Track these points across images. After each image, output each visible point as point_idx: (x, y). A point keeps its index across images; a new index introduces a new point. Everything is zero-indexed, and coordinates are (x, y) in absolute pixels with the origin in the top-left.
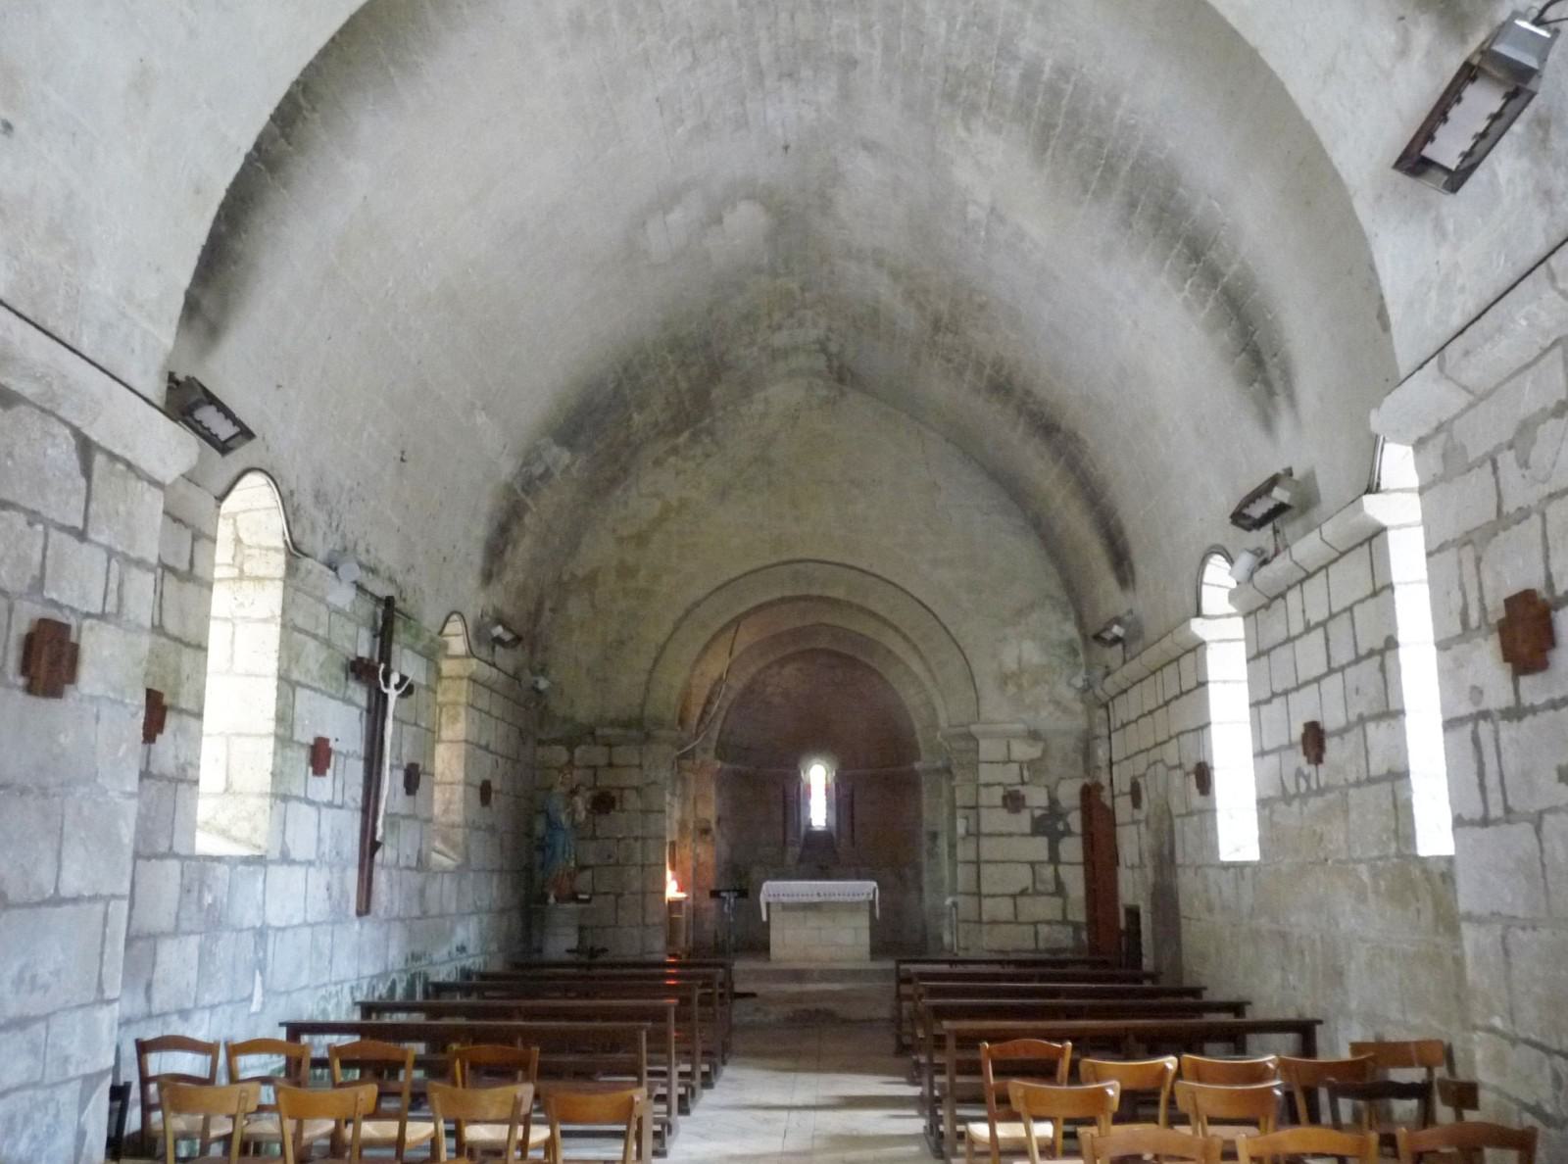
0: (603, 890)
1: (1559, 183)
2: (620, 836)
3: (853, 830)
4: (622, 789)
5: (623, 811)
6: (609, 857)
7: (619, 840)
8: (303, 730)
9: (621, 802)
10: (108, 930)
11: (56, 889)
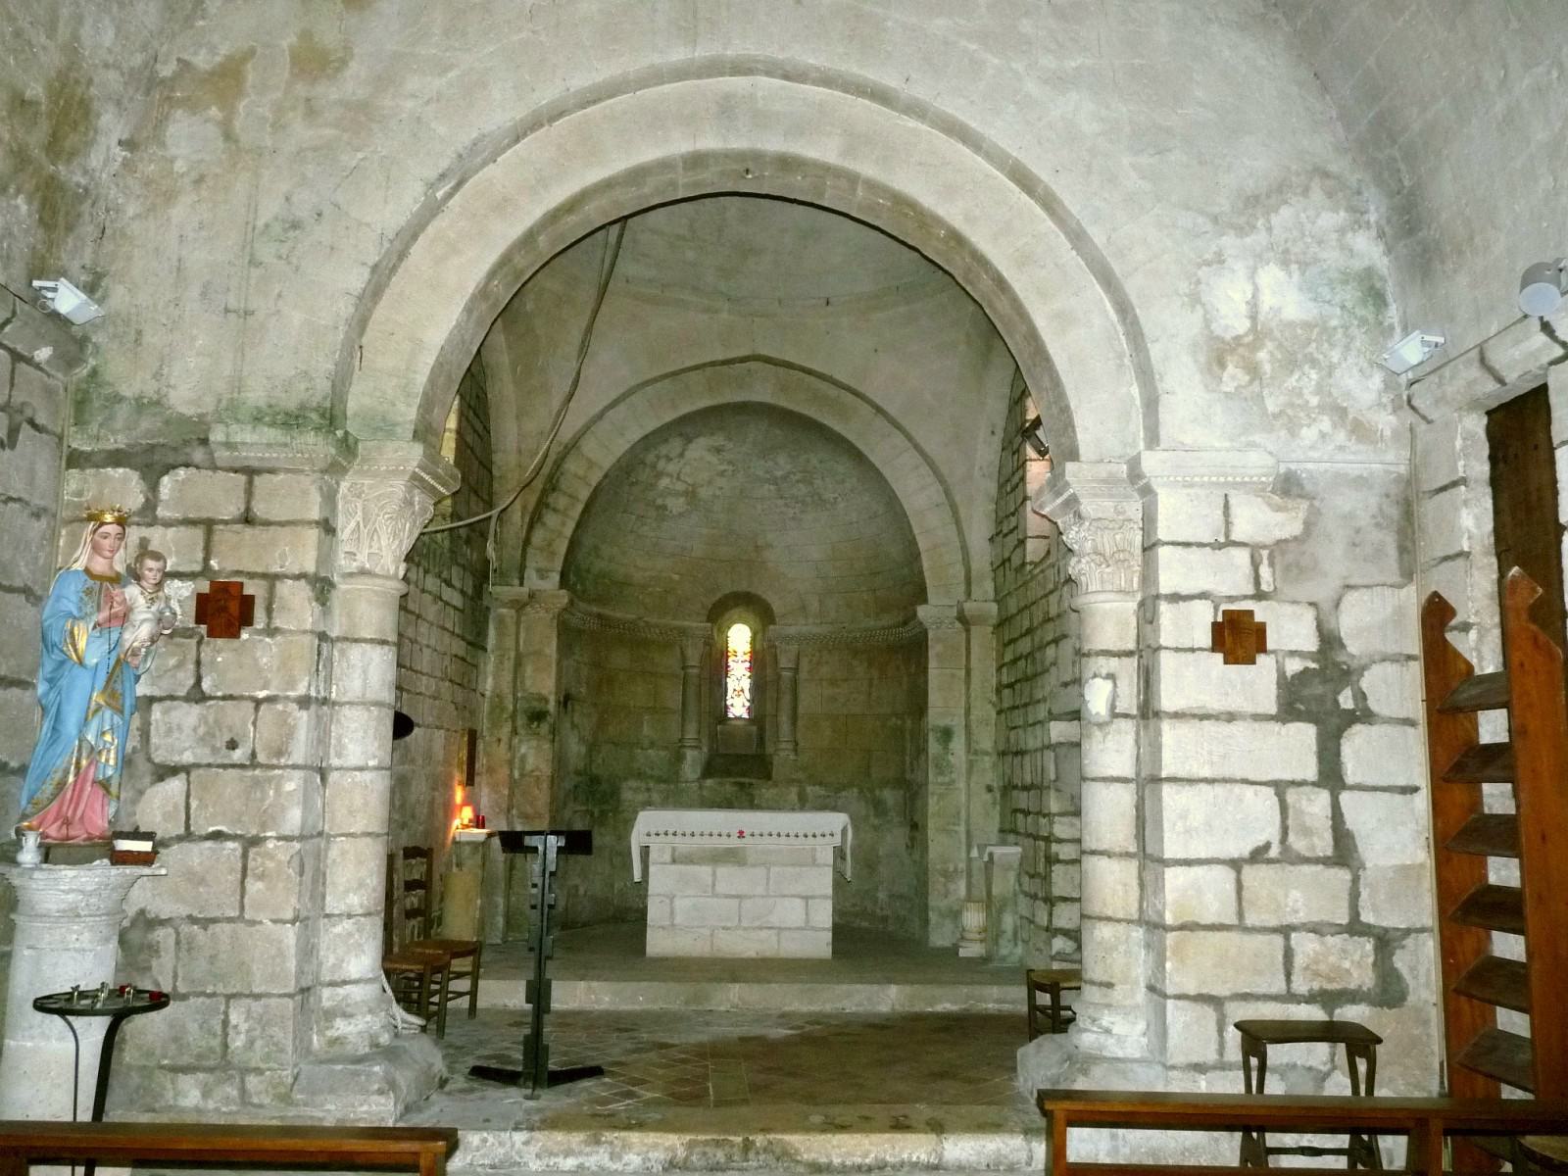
2: (261, 694)
4: (272, 579)
5: (271, 631)
6: (232, 745)
7: (258, 703)
9: (269, 611)
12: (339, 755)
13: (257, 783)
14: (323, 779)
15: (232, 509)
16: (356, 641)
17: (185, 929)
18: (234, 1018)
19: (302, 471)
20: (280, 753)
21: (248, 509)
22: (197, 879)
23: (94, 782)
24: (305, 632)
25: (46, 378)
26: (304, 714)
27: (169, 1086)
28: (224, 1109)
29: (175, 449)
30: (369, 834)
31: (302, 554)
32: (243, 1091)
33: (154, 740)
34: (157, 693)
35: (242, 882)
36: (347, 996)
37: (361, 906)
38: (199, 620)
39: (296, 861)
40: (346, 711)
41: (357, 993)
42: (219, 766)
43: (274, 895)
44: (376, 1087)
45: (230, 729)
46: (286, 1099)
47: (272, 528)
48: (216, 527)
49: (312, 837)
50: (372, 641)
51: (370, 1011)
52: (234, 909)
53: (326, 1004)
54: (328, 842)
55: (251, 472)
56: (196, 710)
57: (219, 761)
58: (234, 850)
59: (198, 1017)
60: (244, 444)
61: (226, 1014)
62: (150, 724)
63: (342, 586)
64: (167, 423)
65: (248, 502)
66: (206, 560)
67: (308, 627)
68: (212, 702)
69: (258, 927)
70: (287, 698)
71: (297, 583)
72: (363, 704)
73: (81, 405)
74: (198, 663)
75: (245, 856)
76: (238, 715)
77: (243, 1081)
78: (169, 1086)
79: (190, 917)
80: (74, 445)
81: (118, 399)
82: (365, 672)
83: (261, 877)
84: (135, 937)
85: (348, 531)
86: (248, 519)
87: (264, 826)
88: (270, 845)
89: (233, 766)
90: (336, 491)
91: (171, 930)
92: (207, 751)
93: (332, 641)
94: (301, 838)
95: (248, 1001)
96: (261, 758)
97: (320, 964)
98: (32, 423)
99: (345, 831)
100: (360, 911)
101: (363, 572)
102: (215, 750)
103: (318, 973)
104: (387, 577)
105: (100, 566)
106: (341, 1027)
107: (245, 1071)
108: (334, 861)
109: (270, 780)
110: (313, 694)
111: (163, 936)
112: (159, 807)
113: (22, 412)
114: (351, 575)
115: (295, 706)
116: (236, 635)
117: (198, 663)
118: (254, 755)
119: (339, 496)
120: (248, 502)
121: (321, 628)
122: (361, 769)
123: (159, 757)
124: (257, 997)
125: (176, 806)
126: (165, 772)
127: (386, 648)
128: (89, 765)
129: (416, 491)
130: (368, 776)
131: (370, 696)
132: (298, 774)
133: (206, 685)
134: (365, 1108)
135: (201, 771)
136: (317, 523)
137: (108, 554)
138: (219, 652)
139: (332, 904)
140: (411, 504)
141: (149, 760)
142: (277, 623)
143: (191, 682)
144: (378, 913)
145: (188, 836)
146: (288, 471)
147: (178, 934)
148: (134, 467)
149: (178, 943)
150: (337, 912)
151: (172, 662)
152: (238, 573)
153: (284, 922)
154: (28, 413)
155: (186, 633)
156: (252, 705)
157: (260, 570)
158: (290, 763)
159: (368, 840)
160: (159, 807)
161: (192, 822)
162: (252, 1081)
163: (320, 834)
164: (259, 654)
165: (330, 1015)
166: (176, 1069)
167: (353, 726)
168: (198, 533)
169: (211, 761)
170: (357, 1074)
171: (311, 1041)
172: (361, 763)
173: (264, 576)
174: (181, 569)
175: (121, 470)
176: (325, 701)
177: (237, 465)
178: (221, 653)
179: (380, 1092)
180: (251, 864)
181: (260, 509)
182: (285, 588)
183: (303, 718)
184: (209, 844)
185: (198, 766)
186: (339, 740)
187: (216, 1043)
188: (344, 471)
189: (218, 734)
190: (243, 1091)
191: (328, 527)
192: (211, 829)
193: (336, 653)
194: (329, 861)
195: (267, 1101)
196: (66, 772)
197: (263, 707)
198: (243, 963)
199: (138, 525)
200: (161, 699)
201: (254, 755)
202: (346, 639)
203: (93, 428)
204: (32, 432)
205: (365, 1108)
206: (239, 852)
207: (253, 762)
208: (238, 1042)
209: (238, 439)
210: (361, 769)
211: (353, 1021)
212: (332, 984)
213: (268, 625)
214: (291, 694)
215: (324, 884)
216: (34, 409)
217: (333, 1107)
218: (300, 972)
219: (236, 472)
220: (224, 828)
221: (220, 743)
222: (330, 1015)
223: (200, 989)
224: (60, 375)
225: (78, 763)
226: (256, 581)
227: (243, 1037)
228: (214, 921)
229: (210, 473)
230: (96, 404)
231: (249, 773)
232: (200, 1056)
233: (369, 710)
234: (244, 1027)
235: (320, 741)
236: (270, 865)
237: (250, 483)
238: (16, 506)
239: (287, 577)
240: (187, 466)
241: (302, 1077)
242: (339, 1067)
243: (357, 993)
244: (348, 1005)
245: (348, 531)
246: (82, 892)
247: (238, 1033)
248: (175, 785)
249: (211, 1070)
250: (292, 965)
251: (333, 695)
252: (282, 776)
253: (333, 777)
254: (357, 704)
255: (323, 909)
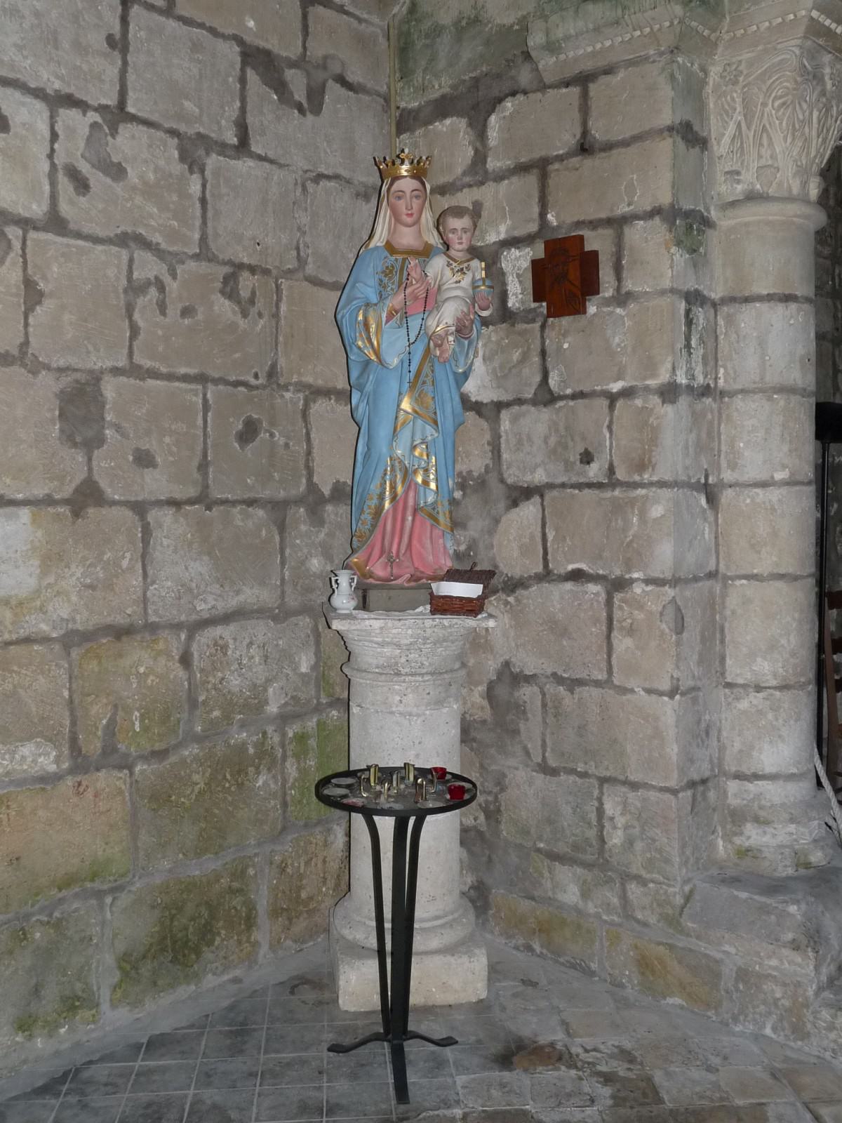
0: (260, 151)
1: (829, 924)
2: (616, 387)
3: (543, 510)
4: (618, 223)
5: (622, 298)
6: (587, 458)
7: (612, 398)
8: (385, 159)
9: (618, 269)
10: (238, 104)
11: (791, 777)
12: (733, 466)
13: (618, 508)
14: (712, 499)
15: (567, 138)
16: (747, 300)
17: (550, 688)
18: (610, 808)
19: (645, 59)
20: (641, 466)
21: (585, 133)
22: (559, 629)
23: (416, 511)
24: (663, 293)
25: (355, 23)
26: (669, 409)
27: (546, 874)
28: (605, 917)
29: (499, 76)
30: (781, 577)
31: (652, 179)
32: (624, 897)
33: (505, 456)
34: (505, 397)
35: (609, 637)
36: (759, 796)
37: (775, 675)
38: (537, 297)
39: (670, 611)
40: (738, 402)
41: (774, 793)
42: (573, 486)
43: (650, 657)
44: (790, 936)
45: (584, 439)
46: (673, 922)
47: (614, 152)
48: (551, 167)
49: (696, 579)
50: (770, 298)
51: (792, 820)
52: (600, 670)
53: (733, 801)
54: (725, 586)
55: (583, 80)
56: (545, 414)
57: (574, 480)
58: (597, 594)
59: (571, 799)
60: (567, 38)
61: (600, 800)
62: (500, 437)
63: (725, 221)
64: (488, 43)
65: (584, 123)
66: (543, 215)
67: (667, 284)
68: (561, 403)
69: (629, 696)
70: (647, 389)
71: (650, 223)
72: (762, 391)
73: (404, 51)
74: (543, 353)
75: (609, 603)
76: (590, 415)
77: (624, 891)
78: (546, 874)
79: (554, 674)
80: (403, 105)
81: (437, 31)
82: (762, 343)
83: (631, 631)
84: (502, 691)
85: (726, 140)
86: (585, 148)
87: (629, 567)
88: (638, 589)
89: (590, 485)
90: (703, 83)
91: (536, 689)
92: (561, 467)
93: (714, 305)
94: (675, 582)
95: (624, 789)
96: (621, 474)
97: (722, 749)
98: (342, 81)
99: (748, 571)
100: (774, 683)
101: (752, 197)
102: (568, 466)
103: (721, 759)
104: (790, 199)
105: (407, 238)
106: (753, 836)
107: (627, 877)
108: (733, 612)
109: (632, 502)
110: (682, 379)
111: (527, 693)
112: (514, 539)
113: (325, 67)
114: (733, 204)
115: (655, 400)
116: (580, 309)
117: (543, 353)
118: (611, 470)
119: (709, 89)
120: (584, 123)
121: (691, 285)
122: (764, 485)
123: (512, 476)
124: (634, 786)
125: (532, 537)
126: (520, 494)
127: (793, 306)
128: (406, 493)
129: (827, 58)
130: (774, 495)
131: (772, 378)
132: (666, 493)
133: (553, 382)
134: (774, 962)
135: (555, 493)
136: (670, 129)
137: (409, 220)
138: (564, 335)
139: (736, 671)
140: (817, 77)
141: (502, 481)
142: (629, 285)
143: (537, 378)
144: (802, 686)
145: (546, 575)
146: (631, 63)
147: (544, 695)
148: (460, 114)
149: (544, 705)
150: (740, 681)
151: (516, 355)
152: (579, 224)
153: (661, 694)
154: (337, 69)
155: (528, 316)
156: (605, 403)
157: (603, 215)
158: (655, 479)
159: (780, 584)
160: (514, 539)
161: (549, 557)
162: (634, 889)
163: (712, 575)
164: (609, 332)
165: (737, 817)
166: (554, 857)
167: (749, 423)
168: (532, 180)
169: (563, 479)
170: (764, 910)
171: (712, 845)
172: (763, 476)
173: (608, 222)
174: (517, 233)
175: (448, 121)
176: (706, 391)
177: (569, 74)
178: (566, 334)
179: (795, 946)
180: (617, 614)
181: (599, 132)
182: (636, 234)
183: (671, 416)
184: (569, 586)
185: (551, 486)
186: (732, 445)
187: (592, 833)
188: (710, 45)
189: (571, 444)
190: (624, 897)
191: (691, 136)
192: (570, 567)
193: (721, 322)
194: (728, 613)
195: (652, 920)
196: (381, 497)
197: (619, 404)
198: (615, 741)
199: (470, 186)
200: (508, 405)
201: (611, 470)
202: (733, 300)
203: (418, 78)
204: (343, 92)
205: (774, 962)
206: (603, 597)
207: (611, 482)
208: (616, 839)
209: (559, 33)
210: (764, 485)
211: (770, 830)
212: (739, 776)
213: (618, 289)
214: (652, 383)
215: (722, 641)
216: (343, 64)
217: (733, 950)
218: (689, 759)
219: (567, 85)
220: (583, 566)
221: (574, 457)
222: (737, 817)
223: (571, 765)
224: (375, 19)
225: (393, 488)
226: (600, 231)
227: (620, 833)
228: (580, 682)
229: (539, 95)
230: (419, 45)
231: (608, 494)
232: (576, 847)
233: (770, 399)
234: (621, 821)
235: (701, 448)
236: (640, 616)
237: (585, 95)
238: (332, 184)
239: (636, 217)
240: (513, 94)
241: (697, 897)
242: (744, 895)
243: (774, 793)
244: (761, 808)
245: (726, 140)
246: (398, 646)
247: (615, 828)
248: (529, 511)
249: (588, 866)
250: (673, 750)
251: (721, 382)
252: (646, 496)
253: (727, 496)
254: (753, 392)
255: (723, 674)
